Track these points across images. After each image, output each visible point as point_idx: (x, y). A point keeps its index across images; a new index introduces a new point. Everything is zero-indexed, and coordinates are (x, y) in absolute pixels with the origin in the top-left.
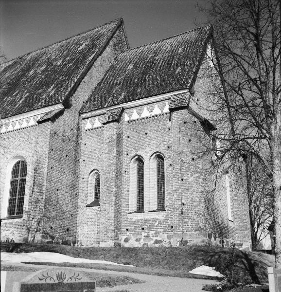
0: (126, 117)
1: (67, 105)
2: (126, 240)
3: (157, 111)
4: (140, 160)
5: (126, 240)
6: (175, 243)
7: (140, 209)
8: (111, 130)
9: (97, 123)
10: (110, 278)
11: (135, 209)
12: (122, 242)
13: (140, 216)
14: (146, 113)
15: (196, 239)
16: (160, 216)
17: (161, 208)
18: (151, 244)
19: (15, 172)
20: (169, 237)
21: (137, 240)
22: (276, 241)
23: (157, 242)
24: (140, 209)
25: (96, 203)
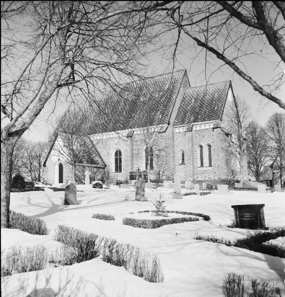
0: (194, 129)
1: (169, 124)
2: (197, 178)
3: (207, 127)
4: (201, 147)
5: (197, 178)
6: (216, 178)
7: (202, 165)
8: (189, 134)
9: (181, 130)
10: (26, 289)
11: (208, 165)
12: (196, 179)
13: (202, 169)
14: (203, 127)
15: (223, 177)
16: (210, 168)
17: (210, 165)
18: (207, 179)
19: (116, 154)
20: (214, 176)
21: (202, 177)
22: (224, 255)
23: (209, 178)
24: (202, 165)
25: (183, 163)
